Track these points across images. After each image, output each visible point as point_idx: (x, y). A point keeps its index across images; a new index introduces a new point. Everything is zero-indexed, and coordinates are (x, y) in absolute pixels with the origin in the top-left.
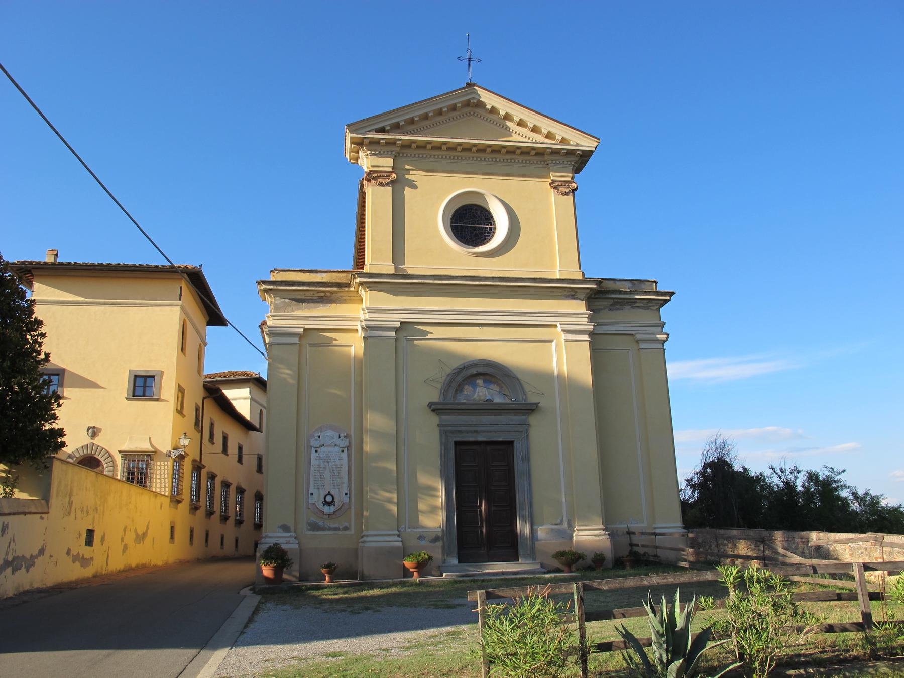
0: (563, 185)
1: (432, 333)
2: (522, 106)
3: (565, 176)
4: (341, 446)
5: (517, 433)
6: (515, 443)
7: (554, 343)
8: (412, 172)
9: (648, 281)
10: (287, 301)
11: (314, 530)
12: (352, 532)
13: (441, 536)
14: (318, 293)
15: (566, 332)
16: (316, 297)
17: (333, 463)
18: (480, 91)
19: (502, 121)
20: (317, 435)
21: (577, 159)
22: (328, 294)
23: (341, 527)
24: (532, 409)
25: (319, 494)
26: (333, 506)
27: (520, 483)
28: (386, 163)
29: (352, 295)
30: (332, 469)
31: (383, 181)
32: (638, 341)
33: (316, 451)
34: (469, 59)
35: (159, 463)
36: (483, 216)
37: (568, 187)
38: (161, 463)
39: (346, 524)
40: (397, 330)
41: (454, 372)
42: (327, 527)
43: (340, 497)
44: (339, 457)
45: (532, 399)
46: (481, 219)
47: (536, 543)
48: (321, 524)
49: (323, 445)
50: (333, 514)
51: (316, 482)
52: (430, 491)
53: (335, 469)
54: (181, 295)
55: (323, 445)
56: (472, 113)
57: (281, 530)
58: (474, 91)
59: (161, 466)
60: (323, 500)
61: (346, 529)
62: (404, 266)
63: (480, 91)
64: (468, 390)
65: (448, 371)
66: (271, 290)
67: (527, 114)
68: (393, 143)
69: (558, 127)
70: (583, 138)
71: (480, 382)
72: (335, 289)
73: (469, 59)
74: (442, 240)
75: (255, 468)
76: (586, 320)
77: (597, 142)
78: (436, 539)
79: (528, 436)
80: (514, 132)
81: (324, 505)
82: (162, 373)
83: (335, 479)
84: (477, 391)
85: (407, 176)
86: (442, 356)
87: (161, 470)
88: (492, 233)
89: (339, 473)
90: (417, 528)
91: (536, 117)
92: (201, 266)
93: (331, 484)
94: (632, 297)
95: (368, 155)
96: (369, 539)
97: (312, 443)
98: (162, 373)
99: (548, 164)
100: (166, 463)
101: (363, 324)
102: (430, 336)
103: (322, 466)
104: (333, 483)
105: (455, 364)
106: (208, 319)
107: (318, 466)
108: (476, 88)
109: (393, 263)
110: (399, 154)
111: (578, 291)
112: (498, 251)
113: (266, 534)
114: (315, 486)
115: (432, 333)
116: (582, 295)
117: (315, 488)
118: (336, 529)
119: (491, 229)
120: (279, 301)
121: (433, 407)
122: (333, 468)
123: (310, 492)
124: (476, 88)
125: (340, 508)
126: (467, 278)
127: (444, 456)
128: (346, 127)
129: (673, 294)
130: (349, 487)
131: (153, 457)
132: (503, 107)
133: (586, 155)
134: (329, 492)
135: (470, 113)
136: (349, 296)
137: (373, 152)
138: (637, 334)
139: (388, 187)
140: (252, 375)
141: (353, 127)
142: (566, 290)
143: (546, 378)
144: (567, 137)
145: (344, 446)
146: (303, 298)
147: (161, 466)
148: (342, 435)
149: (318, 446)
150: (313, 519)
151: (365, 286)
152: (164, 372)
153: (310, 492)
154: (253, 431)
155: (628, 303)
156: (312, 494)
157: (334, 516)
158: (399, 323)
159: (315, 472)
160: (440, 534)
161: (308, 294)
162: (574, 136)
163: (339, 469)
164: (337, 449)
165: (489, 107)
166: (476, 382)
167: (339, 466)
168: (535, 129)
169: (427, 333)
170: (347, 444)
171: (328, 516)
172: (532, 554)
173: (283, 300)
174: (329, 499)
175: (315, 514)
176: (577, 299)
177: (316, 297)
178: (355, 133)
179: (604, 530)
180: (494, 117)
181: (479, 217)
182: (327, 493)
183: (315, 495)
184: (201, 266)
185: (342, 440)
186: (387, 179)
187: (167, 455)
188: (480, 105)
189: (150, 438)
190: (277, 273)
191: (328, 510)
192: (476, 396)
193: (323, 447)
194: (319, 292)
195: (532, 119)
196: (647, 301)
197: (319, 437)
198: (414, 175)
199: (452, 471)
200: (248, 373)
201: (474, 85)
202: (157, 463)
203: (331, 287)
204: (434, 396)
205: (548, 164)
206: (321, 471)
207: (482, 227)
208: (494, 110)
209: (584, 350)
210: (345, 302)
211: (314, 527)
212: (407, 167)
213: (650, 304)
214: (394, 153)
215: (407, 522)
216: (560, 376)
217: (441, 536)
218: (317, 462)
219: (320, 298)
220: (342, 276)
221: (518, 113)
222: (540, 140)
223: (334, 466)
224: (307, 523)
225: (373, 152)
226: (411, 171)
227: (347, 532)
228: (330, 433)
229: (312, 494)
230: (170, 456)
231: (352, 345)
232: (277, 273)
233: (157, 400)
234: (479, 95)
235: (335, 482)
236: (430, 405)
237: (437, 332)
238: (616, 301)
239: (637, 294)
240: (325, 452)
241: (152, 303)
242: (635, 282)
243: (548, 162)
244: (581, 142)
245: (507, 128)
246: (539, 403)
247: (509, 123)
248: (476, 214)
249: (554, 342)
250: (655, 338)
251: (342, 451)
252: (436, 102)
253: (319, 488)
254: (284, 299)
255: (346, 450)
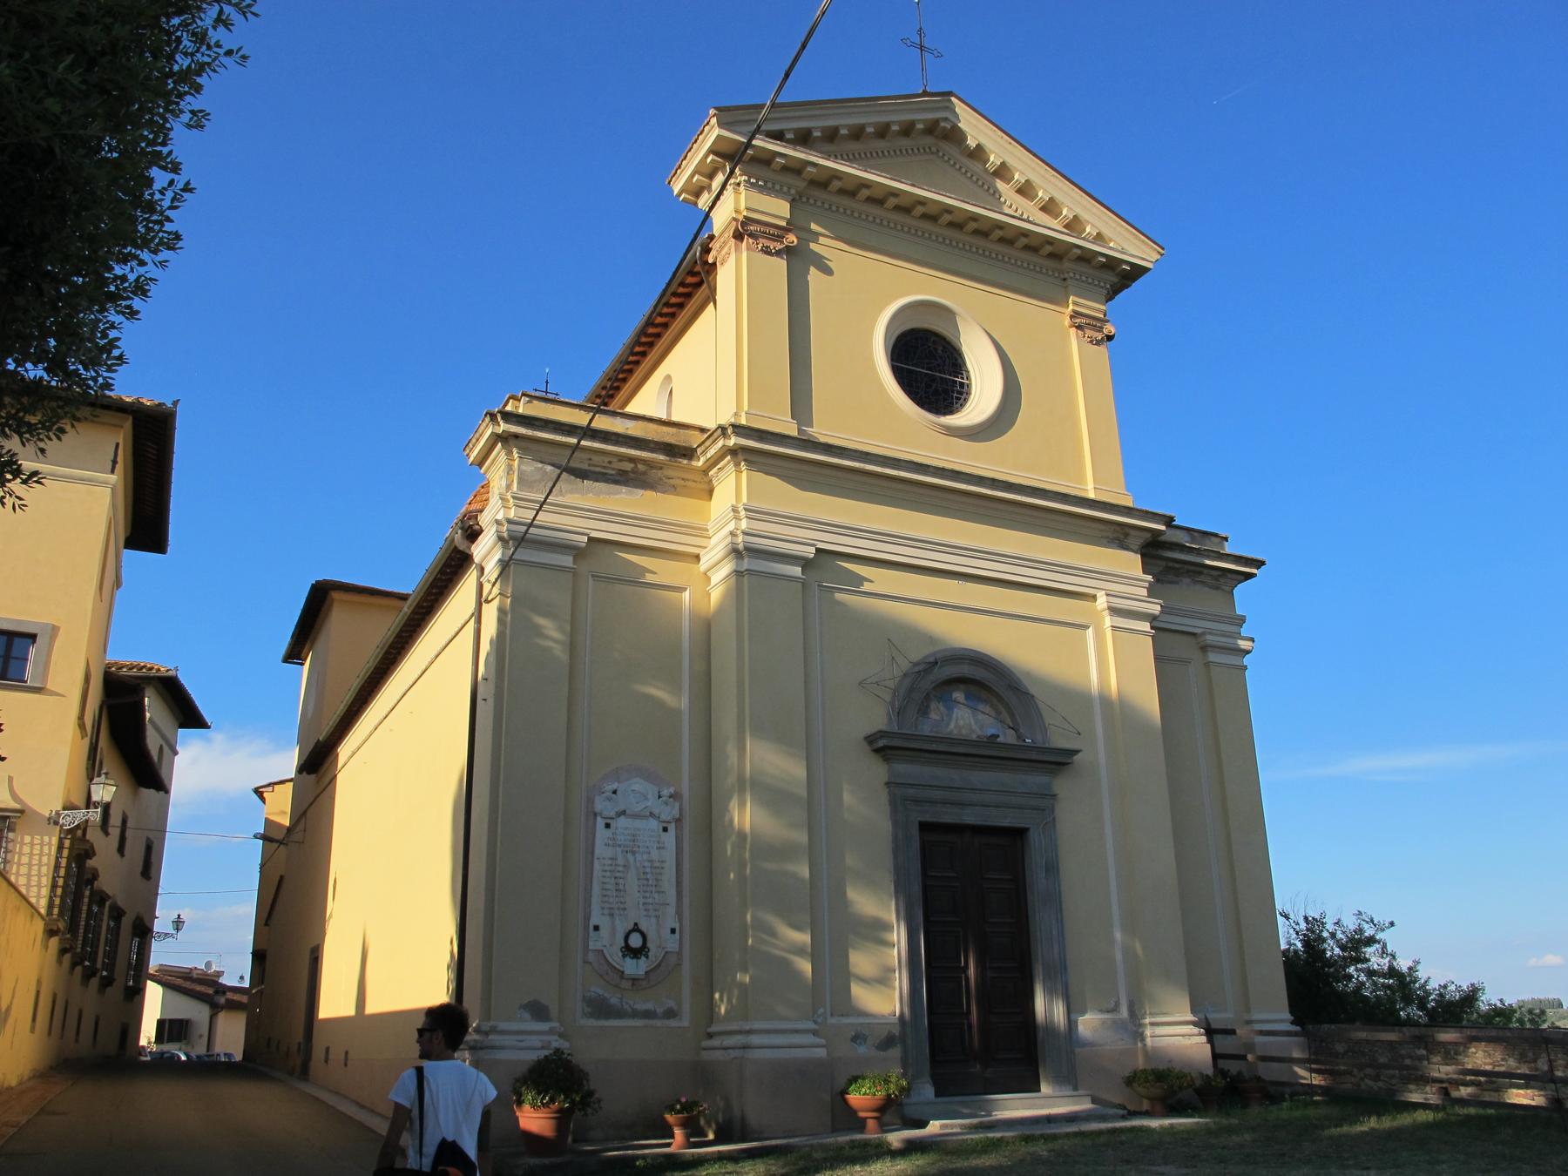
0: (1092, 325)
1: (872, 581)
2: (1035, 155)
3: (1093, 308)
4: (663, 817)
5: (1035, 811)
6: (1031, 832)
7: (1090, 631)
8: (821, 240)
9: (1216, 535)
10: (549, 468)
11: (598, 1018)
12: (686, 1023)
13: (897, 1034)
14: (620, 461)
15: (1114, 611)
16: (613, 469)
17: (645, 857)
18: (960, 108)
19: (989, 178)
20: (609, 787)
21: (1116, 280)
22: (641, 467)
23: (659, 1010)
24: (1059, 761)
25: (613, 929)
26: (643, 958)
27: (1041, 920)
28: (777, 209)
29: (691, 477)
30: (641, 870)
31: (772, 245)
32: (1204, 649)
33: (608, 826)
34: (922, 48)
35: (27, 839)
36: (948, 357)
37: (1100, 330)
38: (32, 839)
39: (671, 1004)
40: (806, 563)
41: (917, 669)
42: (629, 1010)
43: (662, 941)
44: (658, 842)
45: (1060, 740)
46: (944, 362)
47: (1078, 1050)
48: (614, 1001)
49: (624, 813)
50: (643, 977)
51: (606, 899)
52: (874, 932)
53: (648, 870)
54: (115, 462)
55: (624, 813)
56: (934, 149)
57: (527, 1016)
58: (947, 104)
59: (32, 844)
60: (623, 945)
61: (670, 1014)
62: (810, 429)
63: (960, 107)
64: (936, 712)
65: (905, 665)
66: (516, 436)
67: (1042, 172)
68: (796, 169)
69: (1094, 210)
70: (1136, 241)
71: (959, 695)
72: (662, 457)
73: (922, 48)
74: (881, 386)
75: (140, 869)
76: (1145, 592)
77: (1159, 252)
78: (888, 1042)
79: (1054, 819)
80: (1008, 203)
81: (624, 956)
82: (55, 630)
83: (647, 895)
84: (954, 716)
85: (813, 246)
86: (891, 635)
87: (31, 854)
88: (965, 395)
89: (657, 880)
90: (847, 1015)
91: (1057, 182)
92: (175, 403)
93: (641, 906)
94: (1198, 560)
95: (739, 184)
96: (755, 1040)
97: (600, 804)
98: (55, 630)
99: (1065, 279)
100: (46, 839)
101: (740, 539)
102: (866, 587)
103: (620, 861)
104: (644, 904)
105: (918, 654)
106: (128, 534)
107: (610, 862)
108: (953, 99)
109: (792, 418)
110: (801, 197)
111: (1132, 532)
112: (986, 429)
113: (492, 1023)
114: (603, 908)
115: (872, 581)
116: (1136, 541)
117: (603, 914)
118: (648, 1015)
119: (962, 385)
120: (531, 467)
121: (881, 743)
122: (644, 867)
123: (594, 921)
124: (953, 99)
125: (659, 965)
126: (946, 473)
127: (897, 849)
128: (712, 112)
129: (1262, 563)
130: (679, 913)
131: (15, 823)
132: (1001, 151)
133: (1137, 272)
134: (636, 924)
135: (930, 148)
136: (683, 479)
137: (753, 180)
138: (1210, 634)
139: (779, 259)
140: (159, 670)
141: (728, 117)
142: (1113, 527)
143: (1078, 699)
144: (1106, 232)
145: (669, 818)
146: (585, 466)
147: (32, 844)
148: (665, 792)
149: (612, 814)
150: (597, 989)
151: (740, 457)
152: (58, 628)
153: (594, 921)
154: (148, 787)
155: (1188, 571)
156: (596, 928)
157: (644, 983)
158: (813, 550)
159: (604, 877)
160: (896, 1031)
161: (596, 459)
162: (1119, 233)
163: (658, 871)
164: (654, 824)
165: (971, 143)
166: (951, 697)
167: (657, 864)
168: (1050, 207)
169: (861, 580)
170: (676, 813)
171: (630, 982)
172: (1069, 1078)
173: (540, 465)
174: (636, 941)
175: (601, 976)
176: (1126, 548)
177: (613, 469)
178: (728, 130)
179: (1194, 1024)
180: (975, 166)
181: (941, 357)
182: (631, 926)
183: (604, 932)
184: (175, 403)
185: (666, 804)
186: (777, 241)
187: (49, 819)
188: (955, 136)
189: (10, 779)
190: (528, 402)
191: (632, 967)
192: (952, 725)
193: (623, 817)
194: (622, 458)
195: (1049, 185)
196: (1219, 573)
197: (615, 792)
198: (826, 246)
199: (917, 888)
200: (142, 664)
201: (950, 94)
202: (22, 839)
203: (652, 451)
204: (876, 717)
205: (1065, 279)
206: (617, 874)
207: (946, 379)
208: (979, 153)
209: (1144, 650)
210: (674, 490)
211: (601, 1009)
212: (814, 226)
213: (1222, 580)
214: (793, 191)
215: (828, 1005)
216: (1105, 700)
217: (897, 1034)
218: (609, 853)
219: (623, 473)
220: (668, 434)
221: (1025, 167)
222: (1049, 227)
223: (646, 864)
224: (584, 997)
225: (753, 180)
226: (821, 238)
227: (673, 1023)
228: (638, 785)
229: (596, 928)
230: (56, 823)
231: (685, 589)
232: (528, 402)
233: (38, 690)
234: (957, 116)
235: (650, 901)
236: (870, 739)
237: (880, 580)
238: (1171, 564)
239: (1209, 558)
240: (626, 828)
241: (59, 473)
242: (1196, 534)
243: (1066, 276)
244: (1128, 246)
245: (996, 194)
246: (1077, 752)
247: (1000, 185)
248: (936, 349)
249: (1091, 628)
250: (1233, 646)
251: (665, 829)
252: (883, 108)
253: (612, 915)
254: (542, 462)
255: (672, 828)
